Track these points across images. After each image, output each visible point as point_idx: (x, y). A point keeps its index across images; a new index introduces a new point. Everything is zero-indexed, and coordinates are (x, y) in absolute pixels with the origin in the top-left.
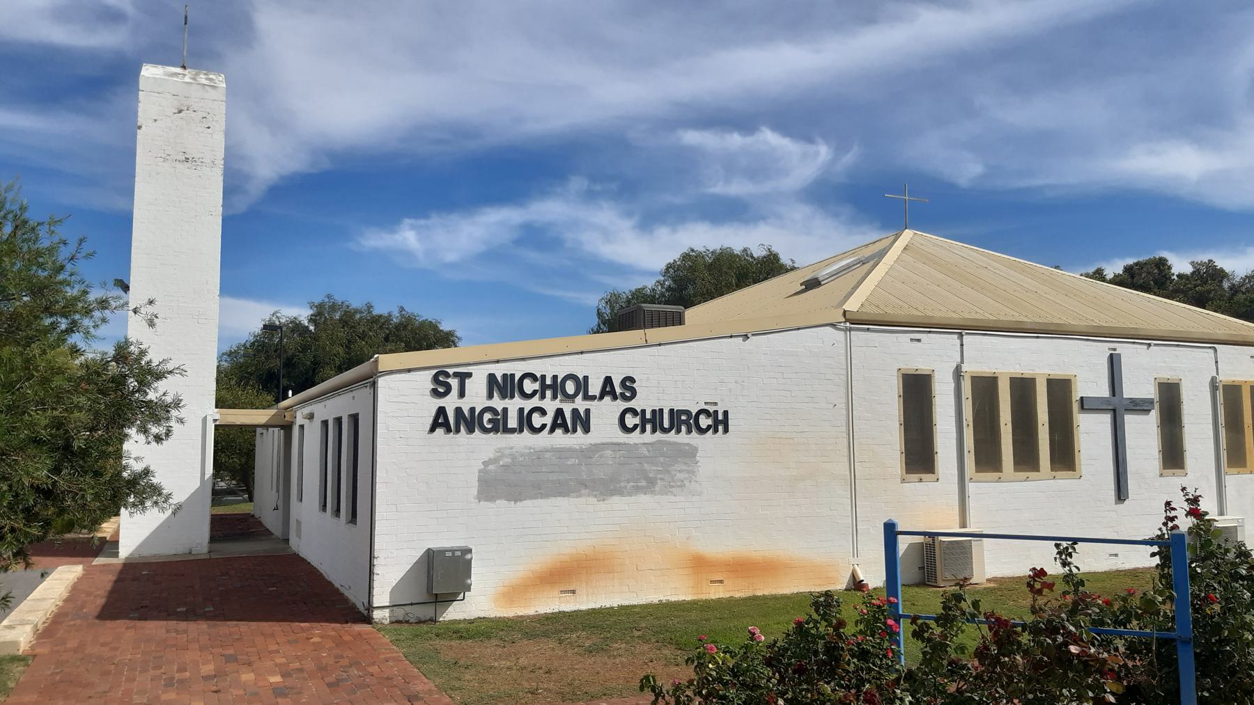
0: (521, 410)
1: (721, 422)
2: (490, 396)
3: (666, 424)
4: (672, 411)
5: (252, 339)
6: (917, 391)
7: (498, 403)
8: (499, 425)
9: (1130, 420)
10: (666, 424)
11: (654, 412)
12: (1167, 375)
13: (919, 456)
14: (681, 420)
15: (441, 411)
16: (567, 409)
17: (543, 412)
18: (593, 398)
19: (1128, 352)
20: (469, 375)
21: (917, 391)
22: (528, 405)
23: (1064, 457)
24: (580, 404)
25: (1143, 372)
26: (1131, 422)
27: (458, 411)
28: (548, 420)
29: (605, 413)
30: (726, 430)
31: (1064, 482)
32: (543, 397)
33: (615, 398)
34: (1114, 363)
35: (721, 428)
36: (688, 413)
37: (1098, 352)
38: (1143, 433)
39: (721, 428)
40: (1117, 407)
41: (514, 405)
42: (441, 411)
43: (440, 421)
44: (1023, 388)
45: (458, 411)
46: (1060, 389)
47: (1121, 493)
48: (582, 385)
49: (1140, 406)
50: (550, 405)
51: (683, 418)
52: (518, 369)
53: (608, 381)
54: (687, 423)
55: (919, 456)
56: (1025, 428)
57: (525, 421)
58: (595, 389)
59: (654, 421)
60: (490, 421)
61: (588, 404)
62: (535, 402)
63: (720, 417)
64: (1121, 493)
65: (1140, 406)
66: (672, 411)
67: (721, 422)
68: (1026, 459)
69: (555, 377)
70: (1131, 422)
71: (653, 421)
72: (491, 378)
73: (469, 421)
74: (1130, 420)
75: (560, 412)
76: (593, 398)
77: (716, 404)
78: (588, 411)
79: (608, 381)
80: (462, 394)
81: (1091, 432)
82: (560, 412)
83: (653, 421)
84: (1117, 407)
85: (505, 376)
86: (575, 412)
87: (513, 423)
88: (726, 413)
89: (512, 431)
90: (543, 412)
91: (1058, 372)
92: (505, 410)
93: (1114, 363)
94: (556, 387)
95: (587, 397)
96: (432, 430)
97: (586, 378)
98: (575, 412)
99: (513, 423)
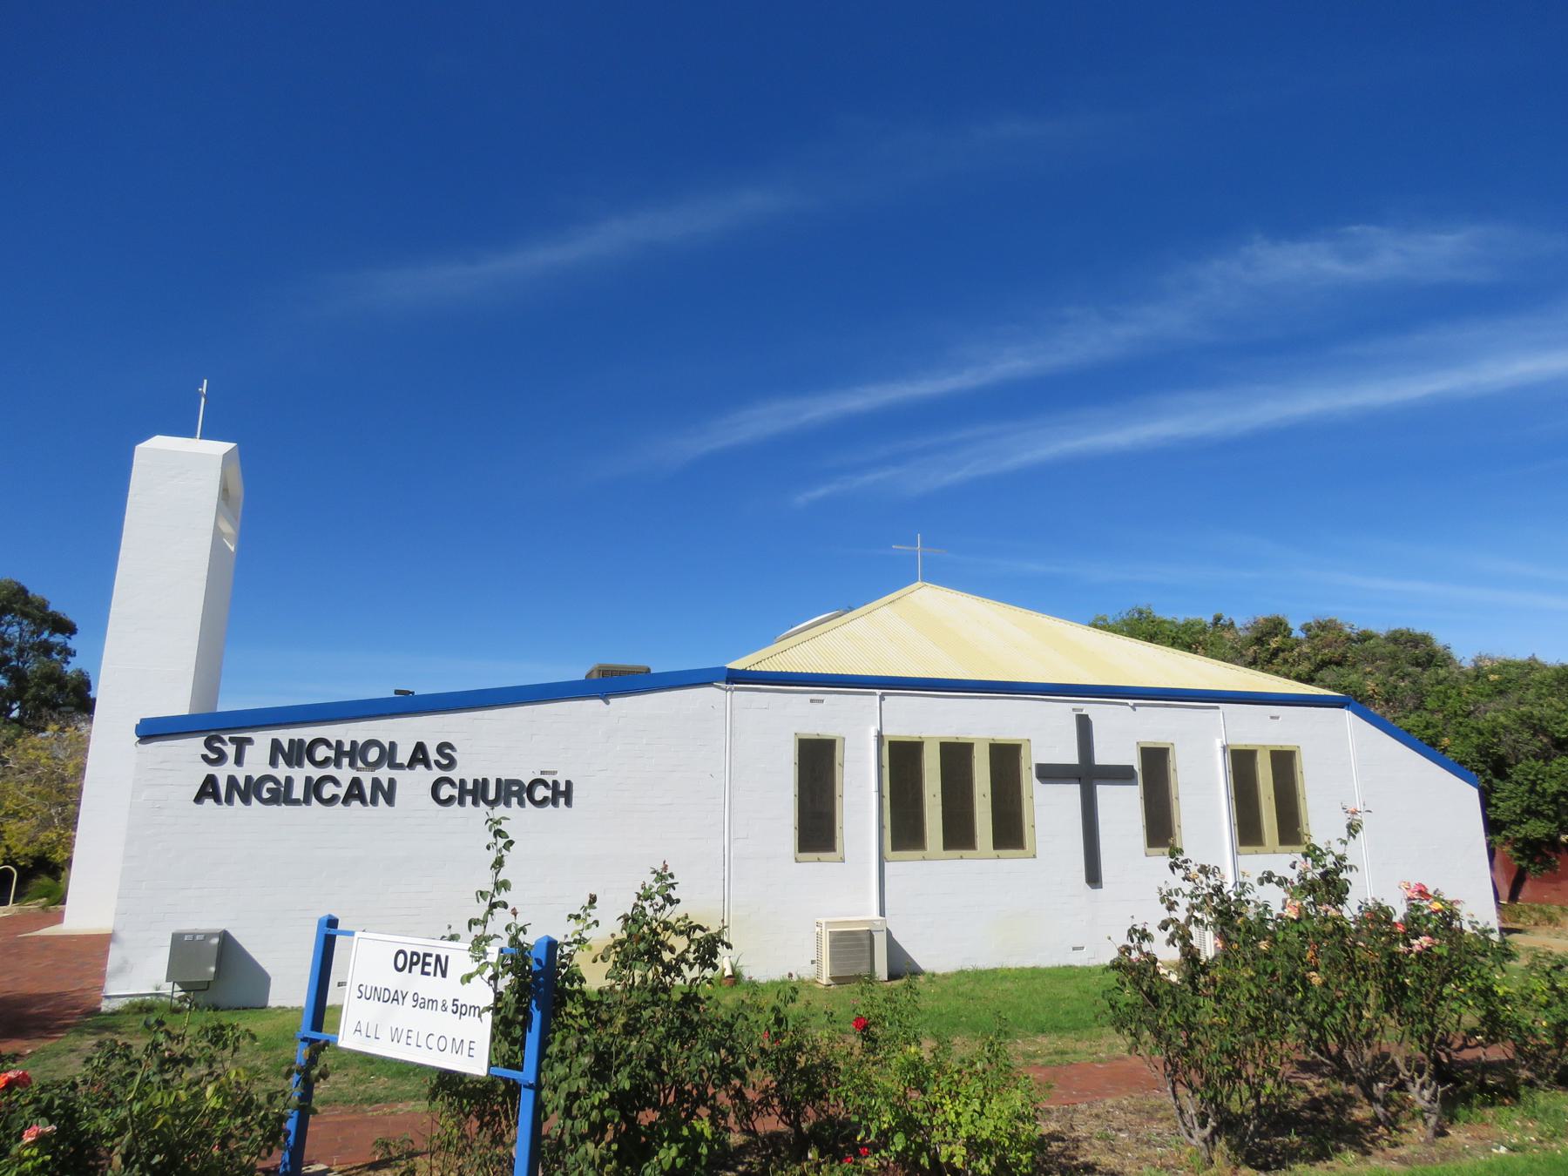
0: (308, 779)
1: (562, 794)
2: (273, 763)
3: (492, 795)
4: (499, 781)
5: (92, 694)
6: (817, 761)
7: (282, 771)
8: (281, 795)
9: (1104, 792)
10: (492, 795)
11: (476, 781)
12: (1155, 739)
13: (817, 829)
14: (510, 791)
15: (211, 780)
16: (366, 779)
17: (336, 782)
18: (401, 766)
19: (1098, 712)
20: (249, 741)
21: (817, 761)
22: (316, 773)
23: (1009, 833)
24: (384, 774)
25: (1120, 735)
26: (1106, 794)
27: (232, 781)
28: (342, 792)
29: (414, 784)
30: (568, 803)
31: (1009, 864)
32: (338, 764)
33: (428, 766)
34: (1084, 725)
35: (562, 801)
36: (518, 782)
37: (1063, 713)
38: (1122, 808)
39: (562, 801)
40: (1087, 774)
41: (301, 774)
42: (211, 780)
43: (208, 790)
44: (956, 756)
45: (232, 781)
46: (1006, 757)
47: (1093, 877)
48: (388, 755)
49: (1120, 775)
50: (345, 774)
51: (515, 788)
52: (307, 734)
53: (420, 747)
54: (518, 795)
55: (817, 829)
56: (954, 799)
57: (314, 789)
58: (403, 756)
59: (478, 792)
60: (269, 790)
61: (394, 774)
62: (331, 770)
63: (562, 788)
64: (1093, 877)
65: (1120, 775)
66: (499, 781)
67: (562, 794)
68: (959, 836)
69: (354, 743)
70: (1106, 794)
71: (473, 793)
72: (276, 745)
73: (248, 791)
74: (1104, 792)
75: (356, 783)
76: (401, 766)
77: (554, 773)
78: (392, 782)
79: (420, 747)
80: (239, 761)
81: (1051, 810)
82: (356, 783)
83: (473, 793)
84: (1087, 774)
85: (291, 742)
86: (376, 783)
87: (298, 792)
88: (569, 784)
89: (297, 802)
90: (336, 782)
91: (1005, 736)
92: (289, 780)
93: (1084, 725)
94: (356, 753)
95: (394, 765)
96: (199, 799)
97: (393, 745)
98: (376, 783)
99: (298, 792)
